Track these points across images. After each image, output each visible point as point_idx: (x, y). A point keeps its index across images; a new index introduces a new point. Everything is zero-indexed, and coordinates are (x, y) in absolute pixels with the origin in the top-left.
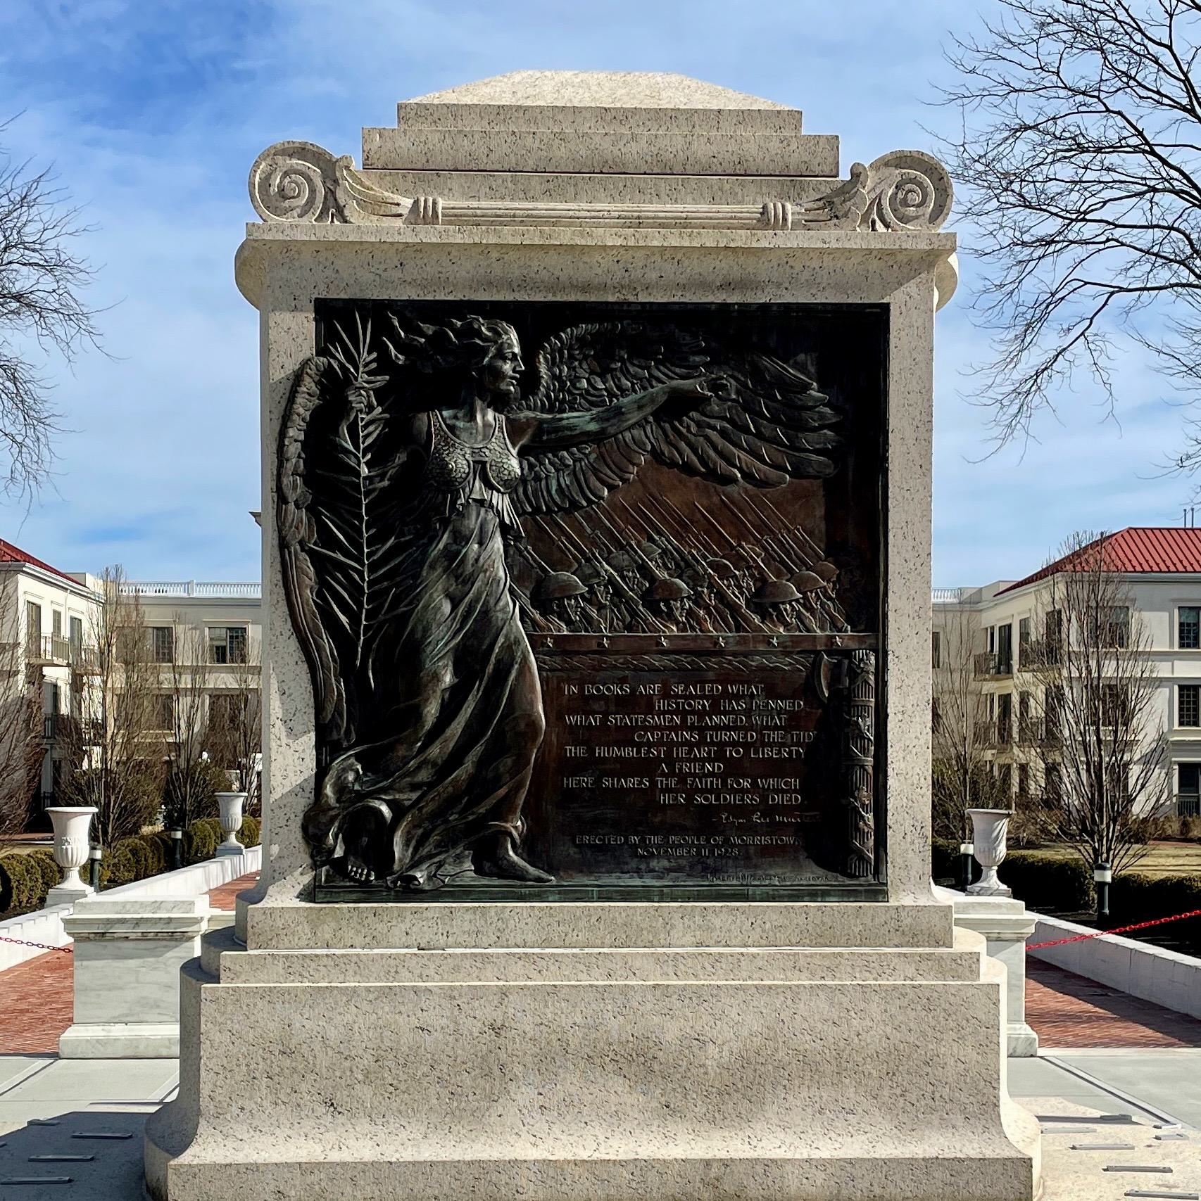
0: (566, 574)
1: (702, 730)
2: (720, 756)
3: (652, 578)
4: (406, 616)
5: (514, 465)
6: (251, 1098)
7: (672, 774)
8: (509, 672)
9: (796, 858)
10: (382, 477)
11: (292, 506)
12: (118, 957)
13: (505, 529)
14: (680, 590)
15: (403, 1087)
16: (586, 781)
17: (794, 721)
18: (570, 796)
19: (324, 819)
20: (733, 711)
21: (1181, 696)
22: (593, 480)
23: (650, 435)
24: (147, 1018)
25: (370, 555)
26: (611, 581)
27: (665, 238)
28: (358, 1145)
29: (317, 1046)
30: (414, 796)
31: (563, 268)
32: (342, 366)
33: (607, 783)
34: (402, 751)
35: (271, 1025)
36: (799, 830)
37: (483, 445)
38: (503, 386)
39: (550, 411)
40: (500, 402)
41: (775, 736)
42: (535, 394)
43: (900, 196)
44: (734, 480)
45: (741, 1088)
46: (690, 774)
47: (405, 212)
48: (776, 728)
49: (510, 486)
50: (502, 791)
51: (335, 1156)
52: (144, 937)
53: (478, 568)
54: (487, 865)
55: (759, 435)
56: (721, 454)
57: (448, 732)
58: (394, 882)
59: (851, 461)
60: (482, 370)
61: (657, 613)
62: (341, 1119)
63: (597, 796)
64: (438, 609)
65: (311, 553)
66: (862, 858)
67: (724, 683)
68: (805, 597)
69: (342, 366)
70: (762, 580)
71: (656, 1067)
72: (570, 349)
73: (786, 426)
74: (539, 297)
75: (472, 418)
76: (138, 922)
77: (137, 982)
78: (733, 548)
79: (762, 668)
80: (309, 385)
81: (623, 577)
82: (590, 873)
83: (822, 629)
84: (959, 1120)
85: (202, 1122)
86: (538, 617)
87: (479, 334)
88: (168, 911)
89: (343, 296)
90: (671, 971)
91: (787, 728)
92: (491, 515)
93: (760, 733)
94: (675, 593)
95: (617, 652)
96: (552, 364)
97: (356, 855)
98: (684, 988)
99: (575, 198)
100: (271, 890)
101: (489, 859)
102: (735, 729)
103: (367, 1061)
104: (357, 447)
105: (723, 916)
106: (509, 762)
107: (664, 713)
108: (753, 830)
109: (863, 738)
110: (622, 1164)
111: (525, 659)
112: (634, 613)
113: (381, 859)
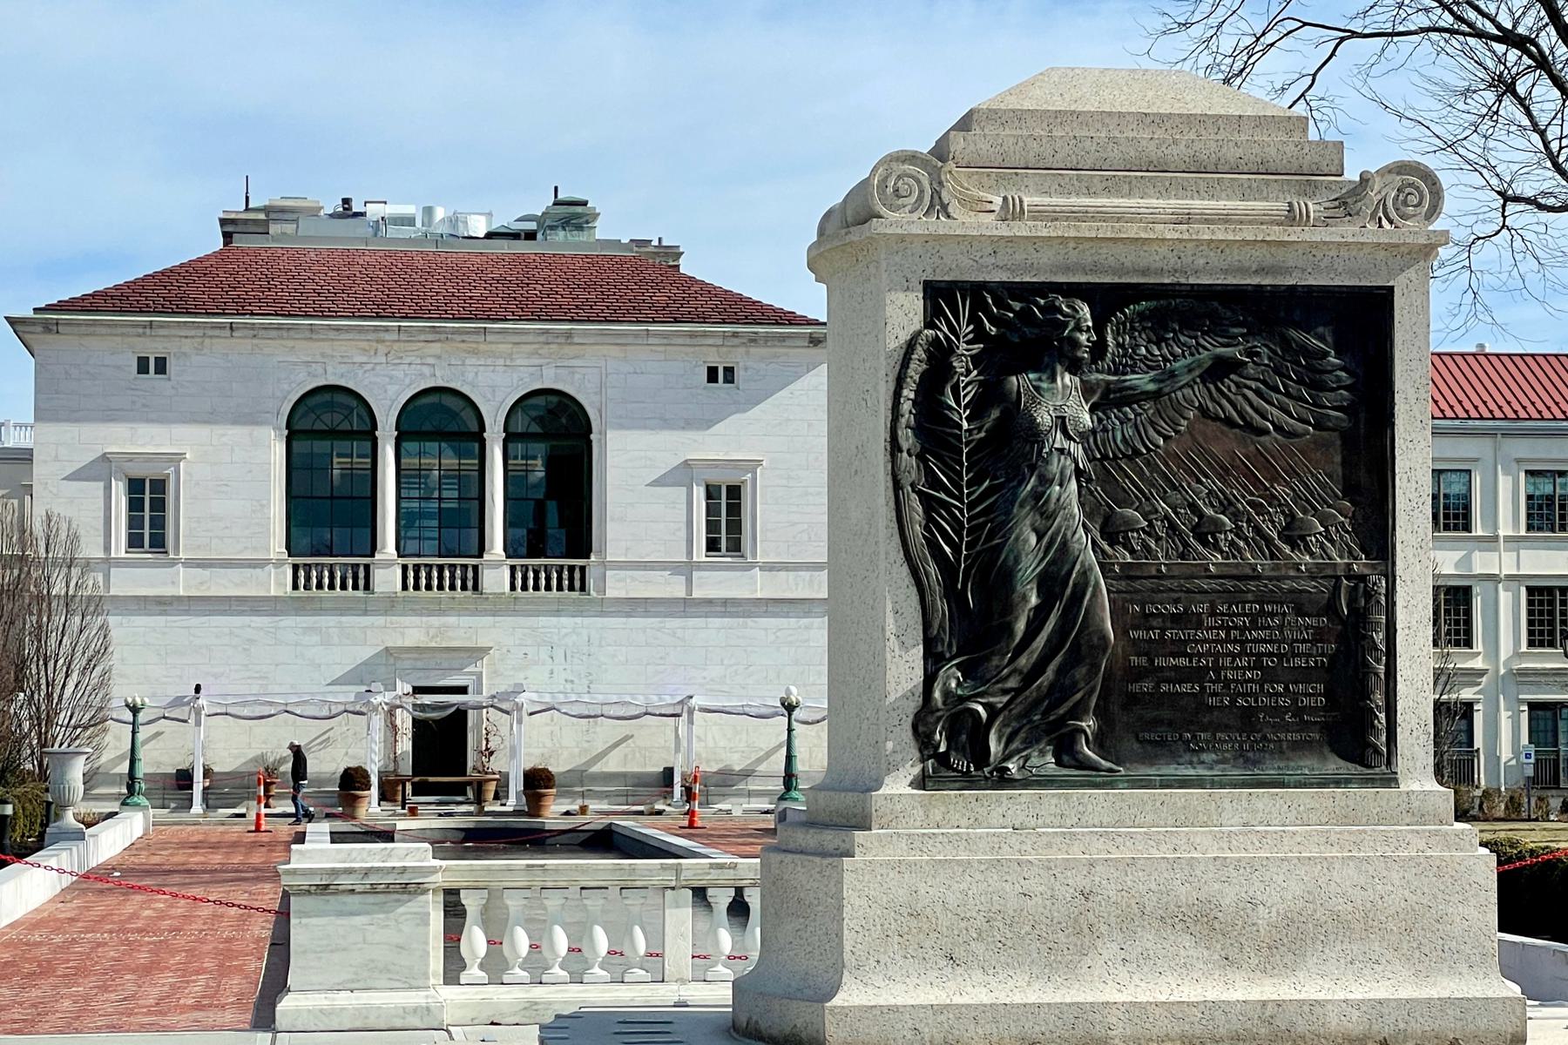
0: (1130, 512)
1: (1243, 643)
2: (1258, 665)
3: (1201, 515)
4: (1000, 547)
5: (1086, 419)
6: (885, 952)
7: (1218, 680)
8: (1084, 594)
9: (1322, 753)
10: (980, 429)
11: (905, 454)
12: (341, 914)
13: (1079, 473)
14: (1224, 524)
15: (1009, 944)
16: (1147, 686)
17: (1319, 636)
18: (1133, 700)
19: (931, 719)
20: (1269, 627)
21: (1530, 603)
22: (1151, 432)
23: (1199, 394)
24: (377, 984)
25: (969, 495)
26: (1167, 517)
27: (1213, 232)
28: (974, 991)
29: (938, 909)
30: (1005, 699)
31: (1129, 257)
32: (947, 337)
33: (1164, 688)
34: (995, 661)
35: (901, 892)
36: (1325, 728)
37: (1061, 402)
38: (1079, 354)
39: (1115, 374)
40: (1074, 367)
41: (1303, 648)
42: (1103, 360)
43: (1401, 198)
44: (1267, 432)
45: (1288, 942)
46: (1233, 681)
47: (997, 209)
48: (1304, 641)
49: (1083, 436)
50: (1079, 696)
51: (958, 1000)
52: (373, 890)
53: (1060, 506)
54: (1066, 758)
55: (1288, 395)
56: (1256, 410)
57: (1035, 645)
58: (991, 773)
59: (1362, 415)
60: (1061, 340)
61: (1205, 544)
62: (959, 970)
63: (1157, 699)
64: (1026, 541)
65: (920, 493)
66: (1377, 752)
67: (1261, 603)
68: (1327, 530)
69: (947, 337)
70: (1291, 516)
71: (1217, 926)
72: (1132, 322)
73: (1309, 386)
74: (1107, 280)
75: (1053, 380)
76: (367, 872)
77: (365, 941)
78: (1266, 489)
79: (1292, 591)
80: (920, 353)
81: (1176, 513)
82: (1152, 765)
83: (1341, 557)
84: (1464, 968)
85: (846, 977)
86: (1107, 547)
87: (1061, 311)
88: (401, 860)
89: (946, 278)
90: (1225, 846)
91: (1313, 642)
92: (1069, 462)
93: (1290, 645)
94: (1218, 527)
95: (1173, 577)
96: (1117, 334)
97: (956, 750)
98: (1239, 860)
99: (1129, 195)
100: (887, 780)
101: (1065, 751)
102: (1270, 642)
103: (980, 921)
104: (958, 404)
105: (1266, 800)
106: (1084, 670)
107: (1212, 628)
108: (1286, 728)
109: (1377, 649)
110: (1194, 1005)
111: (1097, 584)
112: (1186, 545)
113: (980, 755)
